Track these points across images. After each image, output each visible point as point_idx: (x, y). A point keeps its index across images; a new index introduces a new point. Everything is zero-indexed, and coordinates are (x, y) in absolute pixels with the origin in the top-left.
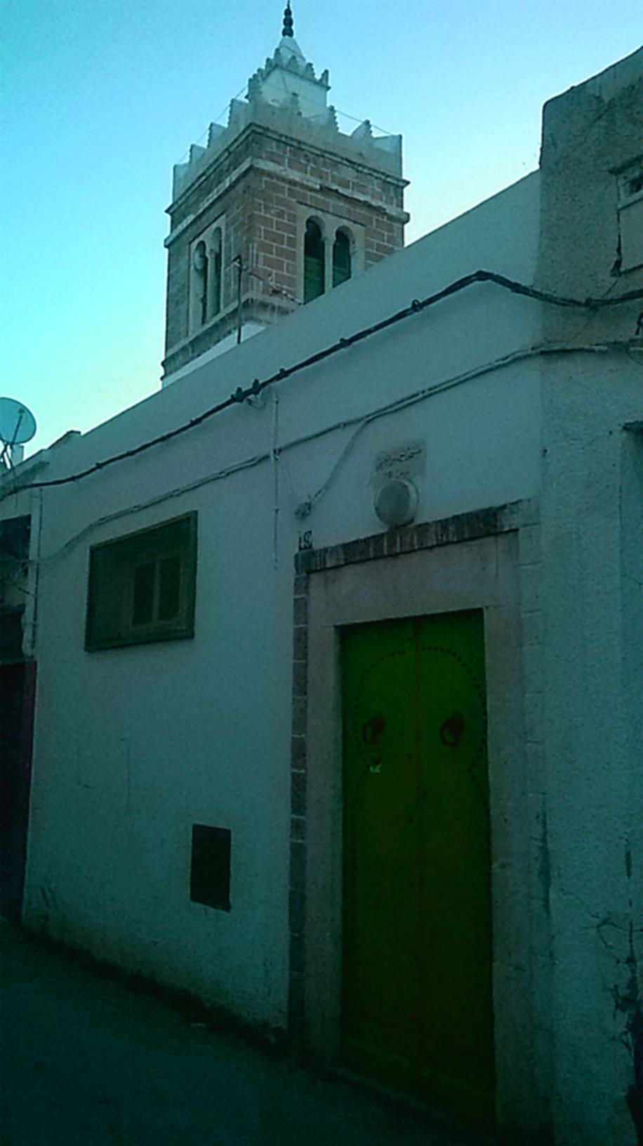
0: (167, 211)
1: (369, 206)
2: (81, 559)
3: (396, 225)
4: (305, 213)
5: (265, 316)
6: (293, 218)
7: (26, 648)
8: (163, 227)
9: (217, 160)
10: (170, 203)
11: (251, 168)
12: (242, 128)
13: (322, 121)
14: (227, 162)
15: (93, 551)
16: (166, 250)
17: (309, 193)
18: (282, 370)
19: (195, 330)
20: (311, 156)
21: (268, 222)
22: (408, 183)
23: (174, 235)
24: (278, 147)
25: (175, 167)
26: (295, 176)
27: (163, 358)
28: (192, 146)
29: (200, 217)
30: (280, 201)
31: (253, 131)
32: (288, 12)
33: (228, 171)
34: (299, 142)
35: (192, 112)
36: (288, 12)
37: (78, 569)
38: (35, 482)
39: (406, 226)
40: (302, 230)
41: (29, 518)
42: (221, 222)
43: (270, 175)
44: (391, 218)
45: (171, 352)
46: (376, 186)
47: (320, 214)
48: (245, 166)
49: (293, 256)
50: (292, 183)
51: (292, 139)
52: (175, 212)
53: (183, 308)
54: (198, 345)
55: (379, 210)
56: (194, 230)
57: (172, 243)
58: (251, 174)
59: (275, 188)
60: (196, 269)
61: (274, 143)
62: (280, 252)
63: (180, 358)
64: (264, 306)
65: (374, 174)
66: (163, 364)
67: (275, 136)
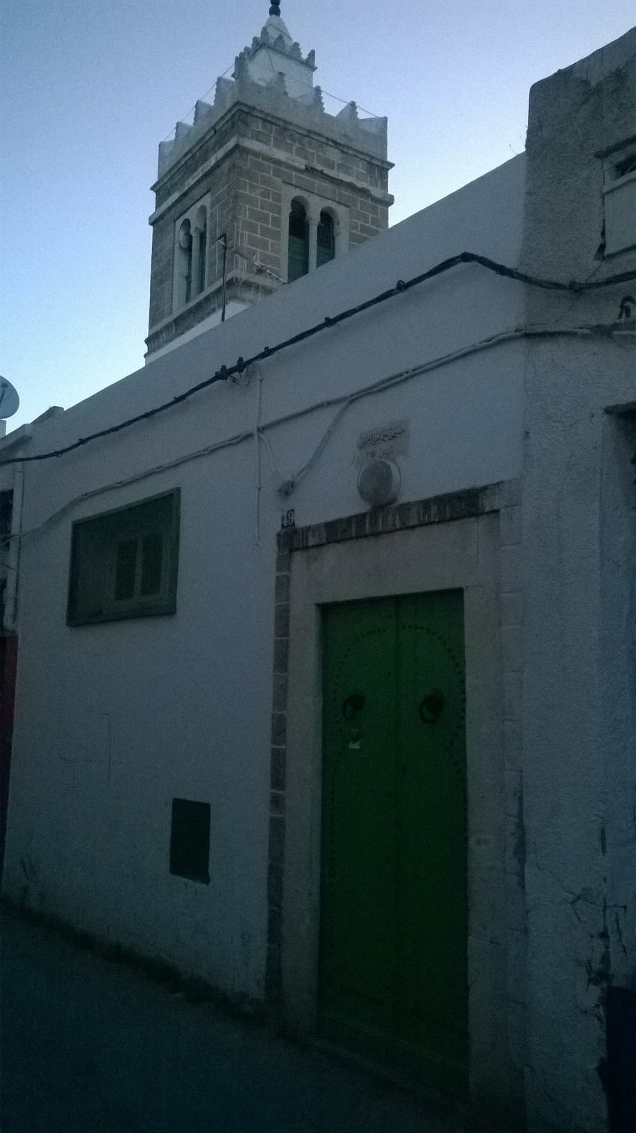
2: (64, 534)
5: (250, 295)
6: (278, 198)
8: (148, 205)
11: (237, 146)
14: (213, 141)
19: (178, 308)
21: (250, 200)
24: (264, 127)
26: (281, 155)
29: (185, 195)
30: (266, 181)
33: (214, 150)
34: (285, 122)
35: (178, 91)
42: (207, 201)
43: (256, 154)
46: (361, 168)
48: (231, 144)
50: (278, 162)
52: (161, 190)
53: (166, 285)
55: (364, 192)
56: (179, 207)
58: (237, 155)
61: (260, 123)
62: (265, 231)
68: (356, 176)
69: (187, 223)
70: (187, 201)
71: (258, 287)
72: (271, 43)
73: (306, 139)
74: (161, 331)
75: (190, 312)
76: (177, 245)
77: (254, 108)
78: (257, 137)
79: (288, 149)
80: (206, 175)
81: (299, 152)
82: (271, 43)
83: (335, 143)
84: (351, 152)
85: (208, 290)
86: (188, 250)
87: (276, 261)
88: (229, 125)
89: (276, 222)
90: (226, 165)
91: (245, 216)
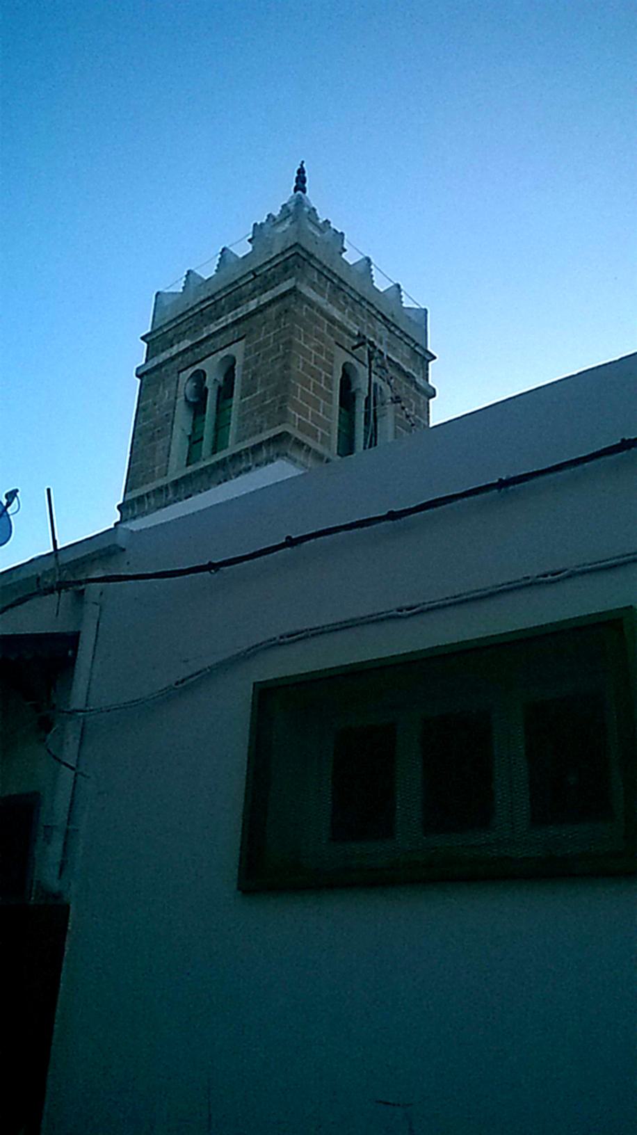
0: (143, 338)
1: (400, 369)
2: (227, 718)
3: (424, 398)
4: (342, 357)
5: (299, 456)
6: (331, 357)
7: (46, 872)
9: (236, 282)
10: (149, 330)
11: (293, 290)
12: (277, 251)
13: (360, 269)
15: (265, 694)
16: (139, 381)
17: (347, 337)
18: (288, 538)
19: (177, 468)
20: (350, 300)
21: (307, 354)
22: (434, 358)
23: (149, 366)
24: (319, 279)
25: (158, 293)
26: (337, 314)
27: (121, 502)
28: (189, 272)
31: (297, 254)
32: (301, 171)
34: (341, 280)
35: (200, 232)
36: (301, 171)
37: (220, 732)
38: (93, 576)
39: (431, 401)
40: (338, 375)
41: (73, 640)
42: (238, 350)
43: (311, 304)
44: (418, 388)
45: (130, 496)
47: (354, 361)
48: (285, 286)
49: (328, 398)
50: (332, 320)
51: (335, 275)
52: (154, 341)
53: (161, 443)
54: (184, 487)
55: (408, 376)
57: (145, 373)
58: (293, 298)
59: (317, 322)
60: (186, 400)
61: (316, 274)
62: (317, 389)
63: (152, 500)
64: (299, 444)
65: (391, 349)
66: (119, 507)
67: (318, 266)
68: (400, 356)
69: (199, 376)
70: (204, 349)
71: (309, 449)
72: (298, 211)
73: (358, 307)
74: (148, 495)
75: (186, 479)
76: (181, 400)
77: (312, 256)
78: (312, 285)
79: (342, 310)
80: (235, 323)
81: (351, 315)
82: (298, 211)
83: (384, 317)
84: (397, 333)
85: (233, 448)
86: (197, 408)
87: (328, 427)
88: (279, 269)
89: (329, 383)
90: (273, 310)
91: (297, 367)
